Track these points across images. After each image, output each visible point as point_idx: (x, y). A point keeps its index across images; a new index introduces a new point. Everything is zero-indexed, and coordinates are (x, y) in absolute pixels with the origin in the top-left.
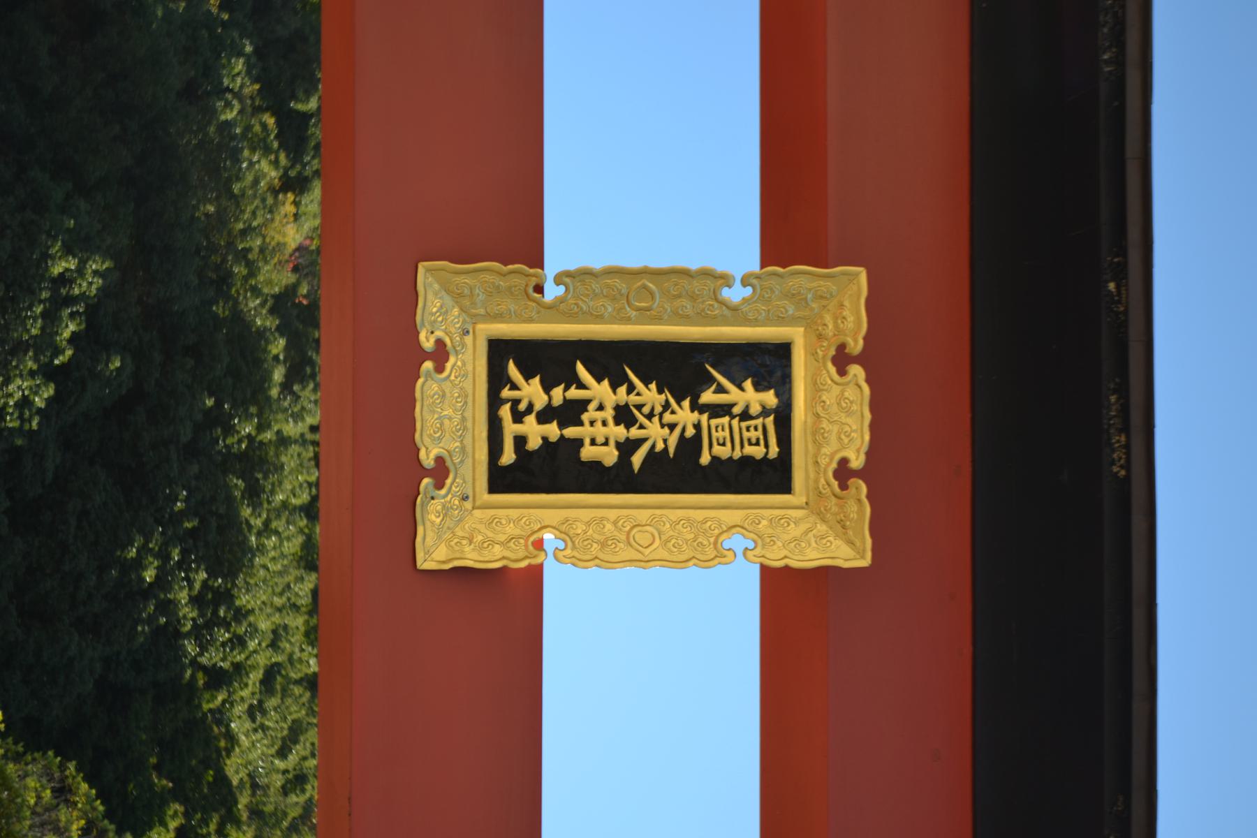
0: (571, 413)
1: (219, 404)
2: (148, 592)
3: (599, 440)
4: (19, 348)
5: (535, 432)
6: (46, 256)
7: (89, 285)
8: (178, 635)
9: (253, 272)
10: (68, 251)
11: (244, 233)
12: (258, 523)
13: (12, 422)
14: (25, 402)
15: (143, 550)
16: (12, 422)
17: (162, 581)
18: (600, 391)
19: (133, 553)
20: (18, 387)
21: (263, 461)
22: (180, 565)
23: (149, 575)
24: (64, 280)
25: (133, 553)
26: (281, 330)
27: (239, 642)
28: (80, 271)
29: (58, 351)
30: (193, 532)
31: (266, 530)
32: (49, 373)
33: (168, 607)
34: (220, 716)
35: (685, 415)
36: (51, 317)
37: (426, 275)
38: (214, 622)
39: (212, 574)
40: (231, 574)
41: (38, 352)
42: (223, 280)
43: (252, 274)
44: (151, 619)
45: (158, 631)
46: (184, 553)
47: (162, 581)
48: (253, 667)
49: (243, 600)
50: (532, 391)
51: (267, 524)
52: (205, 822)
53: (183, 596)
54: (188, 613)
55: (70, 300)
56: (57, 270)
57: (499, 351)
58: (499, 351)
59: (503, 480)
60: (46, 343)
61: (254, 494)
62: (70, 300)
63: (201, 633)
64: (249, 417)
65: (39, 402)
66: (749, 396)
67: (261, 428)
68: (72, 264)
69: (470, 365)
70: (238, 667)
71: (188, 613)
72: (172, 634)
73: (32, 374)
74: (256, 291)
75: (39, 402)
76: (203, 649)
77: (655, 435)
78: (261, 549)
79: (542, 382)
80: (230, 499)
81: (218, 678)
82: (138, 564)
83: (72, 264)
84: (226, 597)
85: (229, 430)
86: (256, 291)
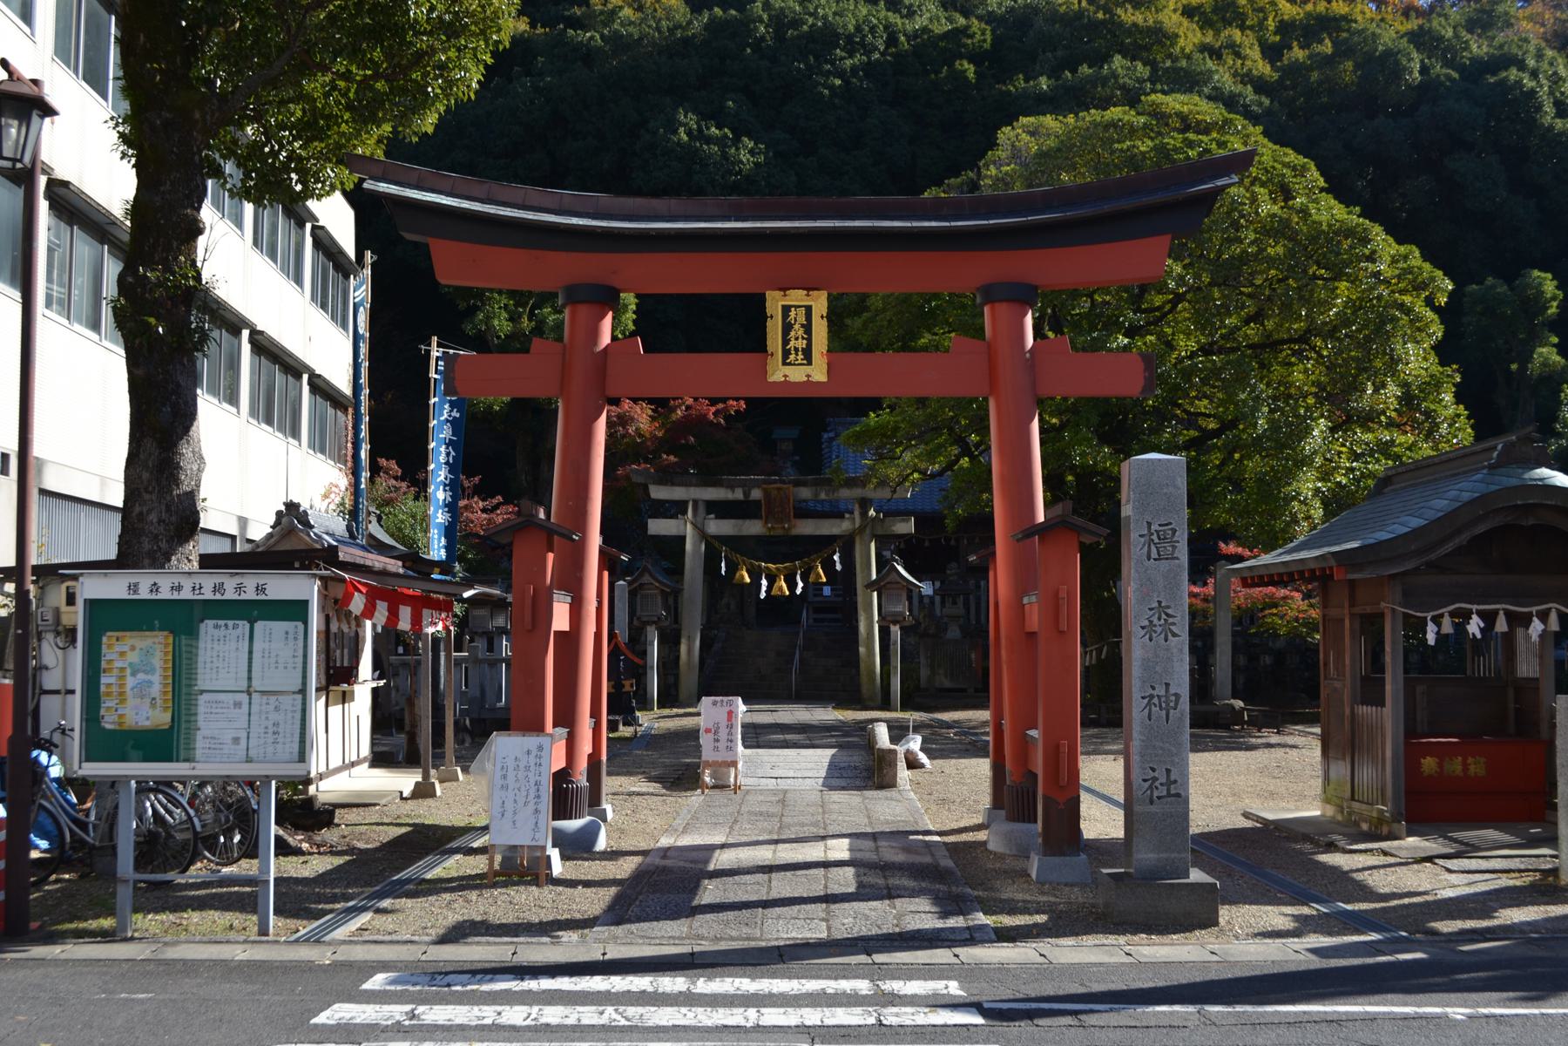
0: (796, 350)
1: (749, 45)
2: (846, 82)
3: (802, 344)
4: (725, 156)
5: (800, 356)
6: (679, 143)
7: (692, 120)
8: (869, 62)
9: (678, 26)
10: (675, 132)
11: (660, 32)
12: (811, 21)
13: (761, 159)
14: (752, 152)
15: (825, 86)
16: (761, 159)
17: (841, 74)
18: (792, 343)
19: (826, 92)
20: (744, 156)
21: (777, 16)
22: (833, 64)
23: (838, 82)
24: (689, 133)
25: (826, 92)
26: (710, 9)
27: (873, 29)
28: (685, 125)
29: (725, 136)
30: (816, 58)
31: (814, 15)
32: (737, 140)
33: (854, 69)
34: (916, 35)
35: (797, 327)
36: (709, 140)
37: (771, 380)
38: (863, 44)
39: (838, 46)
40: (838, 36)
41: (726, 146)
42: (686, 41)
43: (680, 26)
44: (861, 81)
45: (866, 75)
46: (827, 62)
47: (841, 74)
48: (886, 18)
49: (851, 28)
50: (792, 357)
51: (811, 15)
52: (965, 45)
53: (849, 62)
54: (858, 58)
55: (700, 130)
56: (685, 138)
57: (784, 364)
58: (784, 364)
59: (810, 363)
60: (721, 142)
61: (796, 23)
62: (700, 130)
63: (868, 50)
64: (756, 29)
65: (751, 145)
66: (793, 313)
67: (761, 21)
68: (682, 129)
69: (788, 370)
70: (886, 28)
71: (858, 58)
72: (869, 69)
73: (738, 149)
74: (690, 23)
75: (751, 145)
76: (876, 48)
77: (801, 332)
78: (825, 17)
79: (833, 766)
80: (799, 37)
81: (892, 40)
82: (832, 88)
83: (682, 129)
84: (849, 38)
85: (763, 38)
86: (690, 23)
